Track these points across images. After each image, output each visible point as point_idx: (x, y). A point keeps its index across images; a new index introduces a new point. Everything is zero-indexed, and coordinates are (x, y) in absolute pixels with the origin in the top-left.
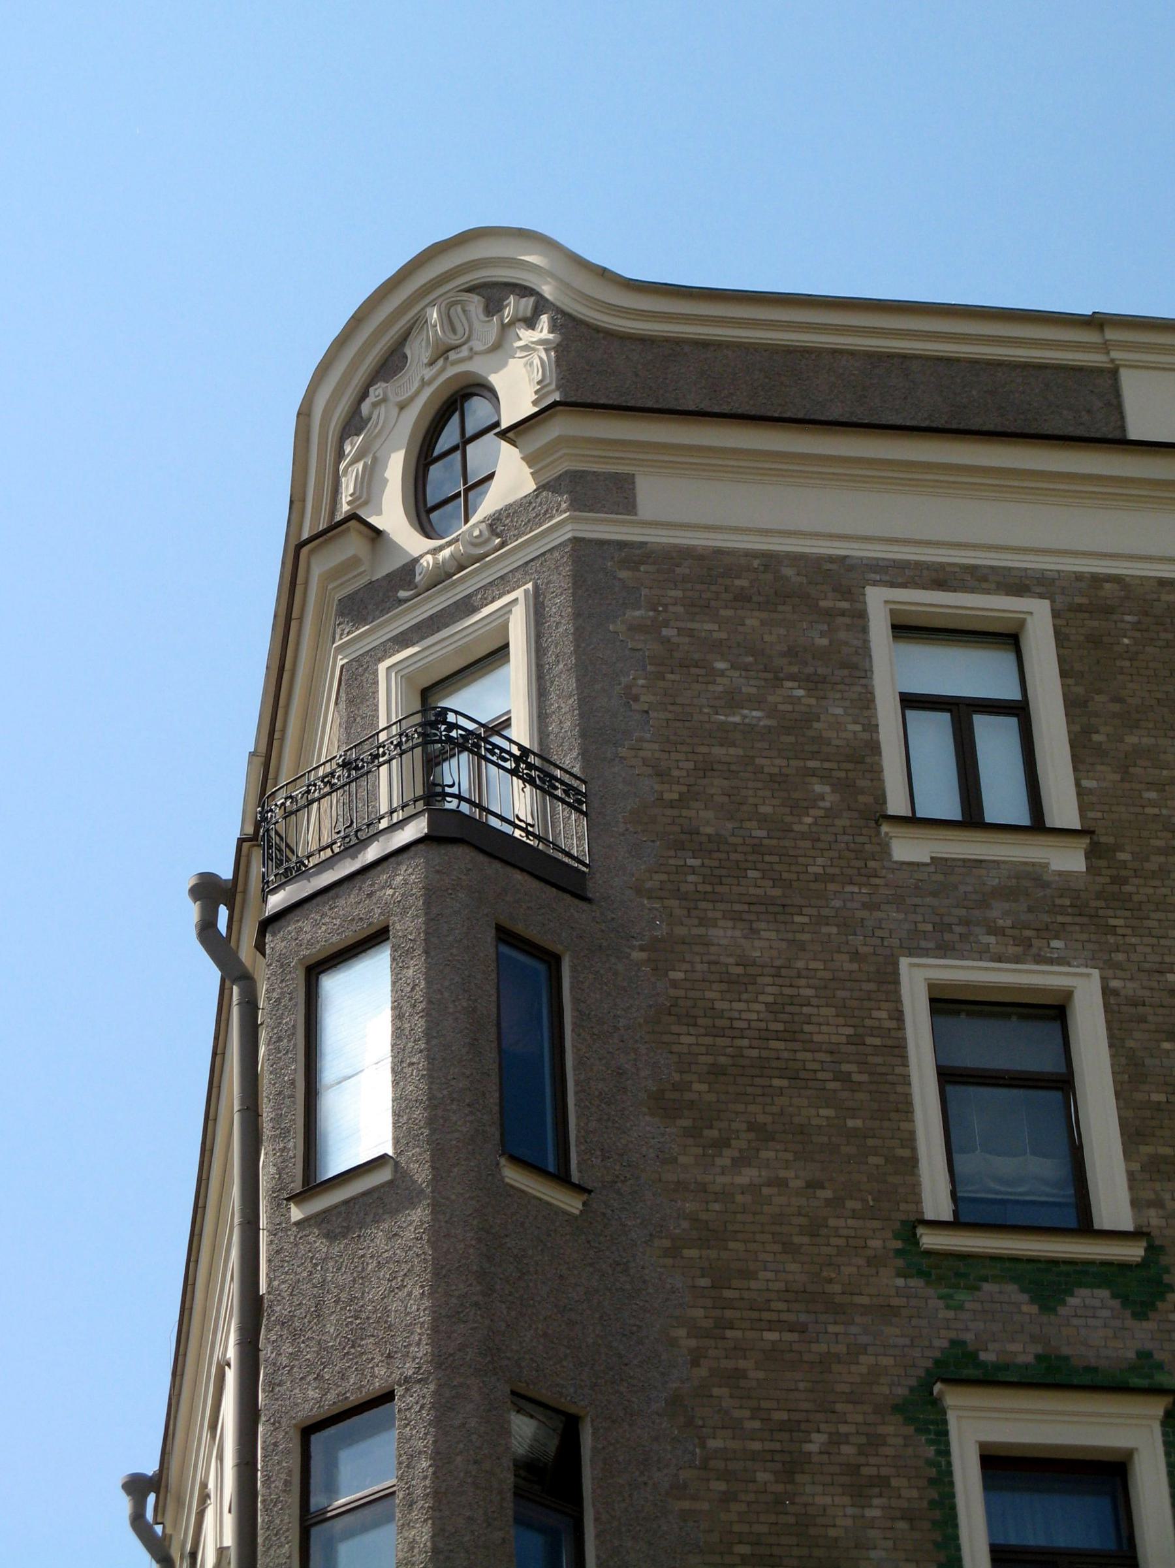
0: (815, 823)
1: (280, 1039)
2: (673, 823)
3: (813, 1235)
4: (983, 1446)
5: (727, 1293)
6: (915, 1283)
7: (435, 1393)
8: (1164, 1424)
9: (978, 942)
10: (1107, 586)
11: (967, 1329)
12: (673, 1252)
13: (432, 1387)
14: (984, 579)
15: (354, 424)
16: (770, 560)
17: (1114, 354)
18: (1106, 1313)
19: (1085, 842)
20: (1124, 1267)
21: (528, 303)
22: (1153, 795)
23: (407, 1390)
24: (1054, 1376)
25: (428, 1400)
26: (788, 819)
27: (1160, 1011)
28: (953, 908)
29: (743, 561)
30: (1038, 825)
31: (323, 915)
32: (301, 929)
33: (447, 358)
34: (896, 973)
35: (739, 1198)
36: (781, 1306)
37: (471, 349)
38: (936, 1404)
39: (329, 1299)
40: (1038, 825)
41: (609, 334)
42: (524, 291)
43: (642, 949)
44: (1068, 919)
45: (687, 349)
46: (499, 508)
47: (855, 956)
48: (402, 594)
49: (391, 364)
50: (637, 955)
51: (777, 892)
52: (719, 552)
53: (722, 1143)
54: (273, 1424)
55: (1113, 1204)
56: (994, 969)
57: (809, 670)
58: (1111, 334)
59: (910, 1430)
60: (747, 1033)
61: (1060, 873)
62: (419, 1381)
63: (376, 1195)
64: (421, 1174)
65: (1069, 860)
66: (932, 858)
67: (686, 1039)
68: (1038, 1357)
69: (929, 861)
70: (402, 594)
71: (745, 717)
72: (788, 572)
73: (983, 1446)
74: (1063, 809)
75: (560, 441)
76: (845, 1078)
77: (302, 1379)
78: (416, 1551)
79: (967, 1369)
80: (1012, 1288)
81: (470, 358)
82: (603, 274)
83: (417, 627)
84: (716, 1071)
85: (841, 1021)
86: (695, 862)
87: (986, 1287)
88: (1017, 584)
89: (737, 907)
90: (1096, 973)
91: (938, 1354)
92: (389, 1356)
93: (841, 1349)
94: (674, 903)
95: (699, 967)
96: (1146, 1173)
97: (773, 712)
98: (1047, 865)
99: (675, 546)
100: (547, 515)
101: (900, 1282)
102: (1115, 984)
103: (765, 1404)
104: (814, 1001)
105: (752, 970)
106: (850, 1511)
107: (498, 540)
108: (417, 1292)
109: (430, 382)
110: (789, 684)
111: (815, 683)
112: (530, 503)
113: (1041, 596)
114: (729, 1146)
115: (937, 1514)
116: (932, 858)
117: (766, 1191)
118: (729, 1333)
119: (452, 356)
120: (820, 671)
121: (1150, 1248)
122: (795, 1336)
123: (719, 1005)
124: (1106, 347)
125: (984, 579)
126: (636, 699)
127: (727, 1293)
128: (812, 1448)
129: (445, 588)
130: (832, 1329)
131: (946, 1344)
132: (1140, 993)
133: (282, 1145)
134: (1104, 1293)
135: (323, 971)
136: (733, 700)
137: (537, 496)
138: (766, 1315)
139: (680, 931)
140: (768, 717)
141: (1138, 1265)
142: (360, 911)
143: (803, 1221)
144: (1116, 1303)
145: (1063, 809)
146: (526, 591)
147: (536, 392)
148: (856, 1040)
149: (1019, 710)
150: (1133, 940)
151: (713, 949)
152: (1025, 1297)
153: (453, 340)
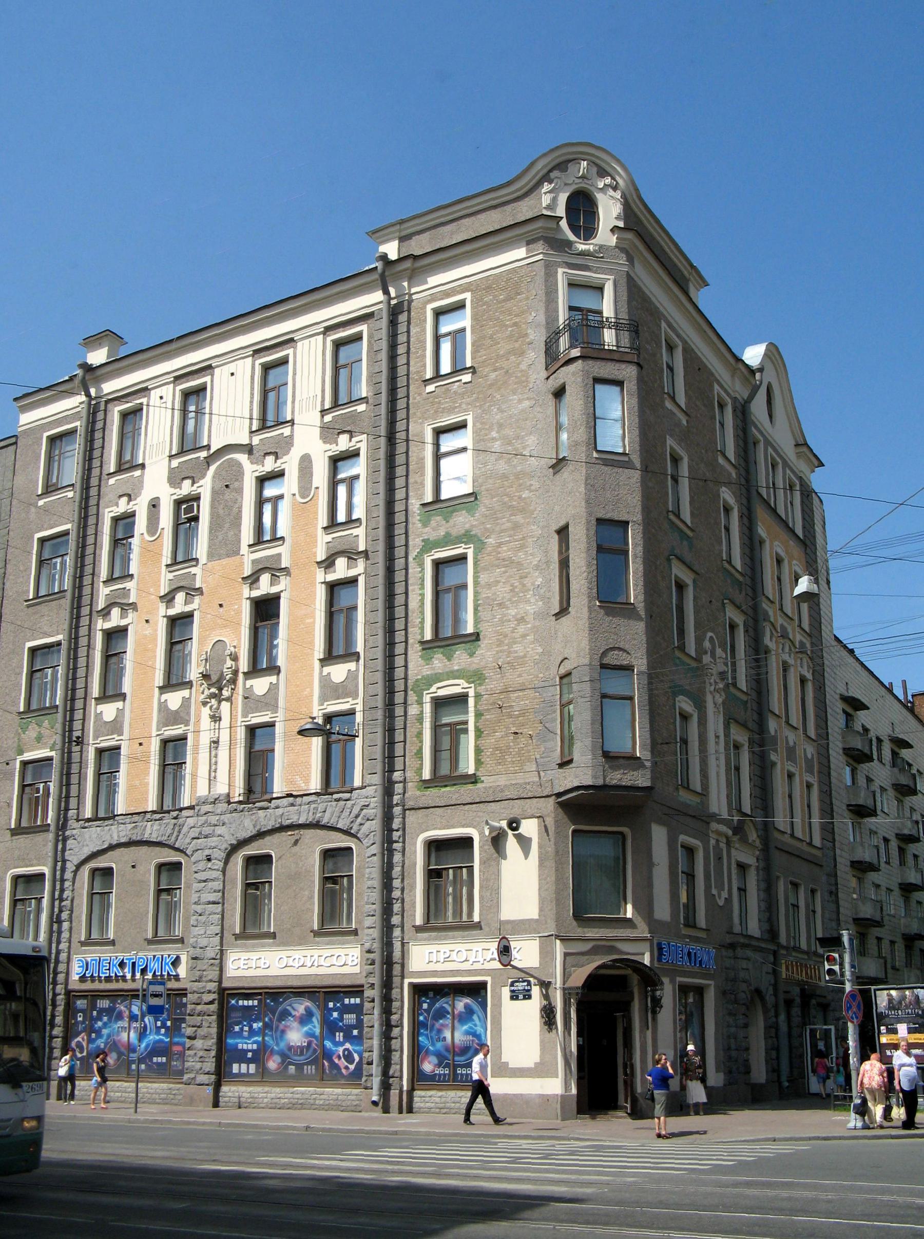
49: (562, 166)
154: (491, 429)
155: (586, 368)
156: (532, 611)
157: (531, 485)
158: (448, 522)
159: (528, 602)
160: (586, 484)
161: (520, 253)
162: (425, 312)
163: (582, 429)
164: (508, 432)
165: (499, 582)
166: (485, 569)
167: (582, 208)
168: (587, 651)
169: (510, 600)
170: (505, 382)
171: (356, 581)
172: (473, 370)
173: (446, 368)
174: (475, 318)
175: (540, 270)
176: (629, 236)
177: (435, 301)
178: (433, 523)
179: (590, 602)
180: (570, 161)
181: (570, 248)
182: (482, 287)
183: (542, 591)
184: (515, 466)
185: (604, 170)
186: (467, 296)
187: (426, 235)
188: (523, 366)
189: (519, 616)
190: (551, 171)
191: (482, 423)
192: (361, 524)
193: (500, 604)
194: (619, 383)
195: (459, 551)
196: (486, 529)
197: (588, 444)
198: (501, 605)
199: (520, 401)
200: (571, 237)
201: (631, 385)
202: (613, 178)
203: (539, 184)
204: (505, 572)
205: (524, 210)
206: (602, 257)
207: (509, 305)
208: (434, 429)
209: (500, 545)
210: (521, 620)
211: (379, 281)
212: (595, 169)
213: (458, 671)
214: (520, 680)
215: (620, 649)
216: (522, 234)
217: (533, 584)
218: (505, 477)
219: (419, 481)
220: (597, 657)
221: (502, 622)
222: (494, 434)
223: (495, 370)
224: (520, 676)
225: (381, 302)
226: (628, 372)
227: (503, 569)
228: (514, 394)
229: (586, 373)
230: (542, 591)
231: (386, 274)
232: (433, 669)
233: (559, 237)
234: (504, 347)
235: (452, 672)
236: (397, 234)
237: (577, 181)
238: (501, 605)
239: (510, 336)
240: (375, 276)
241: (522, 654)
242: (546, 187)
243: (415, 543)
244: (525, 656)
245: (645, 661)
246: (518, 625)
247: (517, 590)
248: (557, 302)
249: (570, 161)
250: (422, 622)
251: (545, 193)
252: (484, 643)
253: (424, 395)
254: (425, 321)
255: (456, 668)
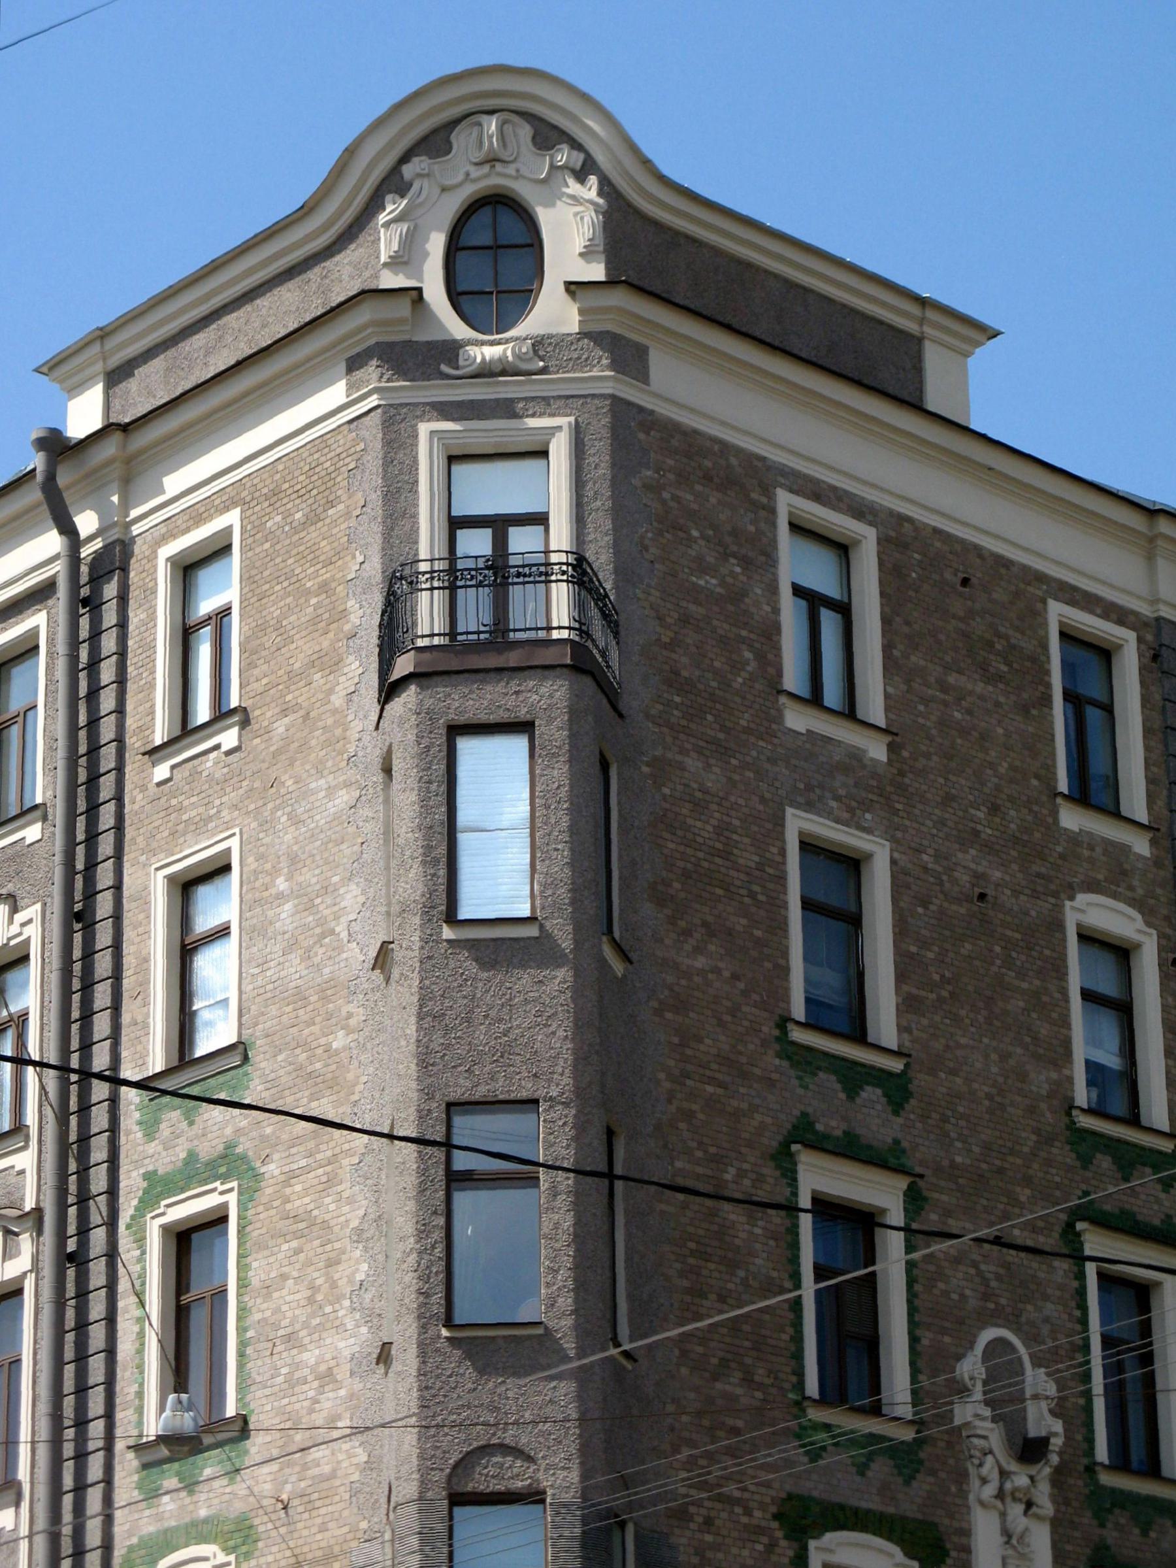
0: (744, 683)
1: (430, 782)
2: (666, 663)
3: (734, 1016)
4: (814, 1191)
5: (689, 1052)
6: (785, 1063)
7: (575, 1116)
8: (905, 1195)
9: (827, 804)
10: (906, 524)
11: (810, 1105)
12: (658, 1012)
13: (573, 1112)
14: (840, 499)
15: (393, 183)
16: (725, 448)
17: (927, 330)
18: (879, 1107)
19: (889, 738)
20: (890, 1074)
21: (578, 159)
22: (921, 708)
23: (551, 1107)
24: (851, 1149)
25: (570, 1120)
26: (729, 676)
27: (919, 882)
28: (824, 776)
29: (708, 444)
30: (850, 712)
31: (471, 692)
32: (450, 695)
33: (494, 166)
34: (783, 818)
35: (696, 979)
36: (714, 1066)
37: (518, 171)
38: (791, 1156)
39: (479, 1012)
40: (850, 712)
41: (637, 212)
42: (576, 145)
43: (648, 765)
44: (875, 798)
45: (682, 241)
46: (542, 333)
47: (763, 800)
48: (445, 368)
49: (435, 142)
50: (645, 769)
51: (721, 736)
52: (696, 432)
53: (687, 933)
54: (427, 1094)
55: (885, 1022)
56: (832, 828)
57: (743, 551)
58: (930, 314)
59: (778, 1173)
60: (703, 847)
61: (872, 759)
62: (563, 1103)
63: (522, 944)
64: (564, 936)
65: (877, 750)
66: (808, 731)
67: (671, 845)
68: (844, 1132)
69: (804, 731)
70: (445, 368)
71: (707, 582)
72: (734, 461)
73: (814, 1191)
74: (874, 707)
75: (620, 310)
76: (752, 895)
77: (454, 1067)
78: (560, 1231)
79: (806, 1134)
80: (833, 1078)
81: (516, 178)
82: (646, 163)
83: (460, 404)
84: (686, 874)
85: (753, 849)
86: (677, 699)
87: (821, 1074)
88: (860, 510)
89: (702, 743)
90: (887, 843)
91: (795, 1121)
92: (535, 1075)
93: (745, 1106)
94: (665, 730)
95: (679, 787)
96: (908, 1005)
97: (722, 583)
98: (865, 751)
99: (671, 420)
100: (587, 363)
101: (777, 1061)
102: (896, 855)
103: (705, 1140)
104: (739, 831)
105: (708, 798)
106: (747, 1227)
107: (541, 364)
108: (561, 1033)
109: (475, 181)
110: (733, 561)
111: (746, 562)
112: (572, 343)
113: (871, 524)
114: (691, 936)
115: (789, 1238)
116: (808, 731)
117: (710, 976)
118: (689, 1082)
119: (499, 167)
120: (750, 554)
121: (907, 1065)
122: (720, 1091)
123: (690, 821)
124: (922, 321)
125: (840, 499)
126: (646, 549)
127: (689, 1052)
128: (728, 1177)
129: (488, 384)
130: (742, 1090)
131: (799, 1114)
132: (909, 866)
133: (432, 871)
134: (879, 1091)
135: (462, 734)
136: (702, 568)
137: (579, 340)
138: (708, 1073)
139: (669, 755)
140: (720, 585)
141: (898, 1075)
142: (511, 702)
143: (729, 1004)
144: (884, 1100)
145: (874, 707)
146: (570, 423)
147: (585, 247)
148: (760, 867)
149: (844, 609)
150: (907, 823)
151: (686, 774)
152: (838, 1086)
153: (504, 155)
154: (275, 872)
155: (429, 702)
156: (347, 1353)
157: (350, 1015)
158: (191, 1123)
159: (340, 1328)
160: (420, 1017)
161: (335, 394)
162: (155, 567)
163: (415, 871)
164: (309, 877)
165: (284, 1277)
166: (261, 1246)
167: (494, 250)
168: (415, 1461)
169: (305, 1325)
170: (304, 746)
171: (19, 1292)
172: (243, 717)
173: (202, 712)
174: (247, 579)
175: (373, 429)
176: (620, 298)
177: (174, 536)
178: (165, 1130)
179: (423, 1328)
180: (456, 122)
181: (453, 362)
182: (252, 493)
183: (368, 1297)
184: (318, 968)
185: (555, 127)
186: (232, 518)
187: (157, 364)
188: (337, 700)
189: (323, 1368)
190: (405, 159)
191: (261, 857)
192: (27, 1139)
193: (289, 1338)
194: (524, 727)
195: (210, 1201)
196: (264, 1138)
197: (427, 910)
198: (290, 1339)
199: (331, 791)
200: (458, 329)
201: (553, 731)
202: (576, 145)
203: (374, 204)
204: (298, 1251)
205: (343, 276)
206: (544, 371)
207: (313, 534)
208: (171, 879)
209: (290, 1177)
210: (327, 1378)
211: (45, 507)
212: (525, 131)
213: (206, 1521)
214: (324, 1539)
215: (505, 1449)
216: (334, 345)
217: (351, 1281)
218: (300, 997)
219: (140, 1019)
220: (438, 1477)
221: (292, 1383)
222: (282, 884)
223: (284, 712)
224: (323, 1528)
225: (56, 557)
226: (548, 697)
227: (294, 1244)
228: (320, 773)
229: (426, 716)
230: (368, 1297)
231: (62, 480)
232: (159, 1517)
233: (424, 336)
234: (303, 649)
235: (194, 1524)
236: (99, 367)
237: (475, 172)
238: (290, 1339)
239: (315, 620)
240: (33, 495)
241: (327, 1469)
242: (392, 207)
243: (131, 1182)
244: (333, 1475)
245: (575, 1476)
246: (321, 1390)
247: (319, 1297)
248: (415, 516)
249: (456, 122)
250: (140, 1394)
251: (387, 225)
252: (256, 1446)
253: (152, 788)
254: (154, 592)
255: (203, 1513)
